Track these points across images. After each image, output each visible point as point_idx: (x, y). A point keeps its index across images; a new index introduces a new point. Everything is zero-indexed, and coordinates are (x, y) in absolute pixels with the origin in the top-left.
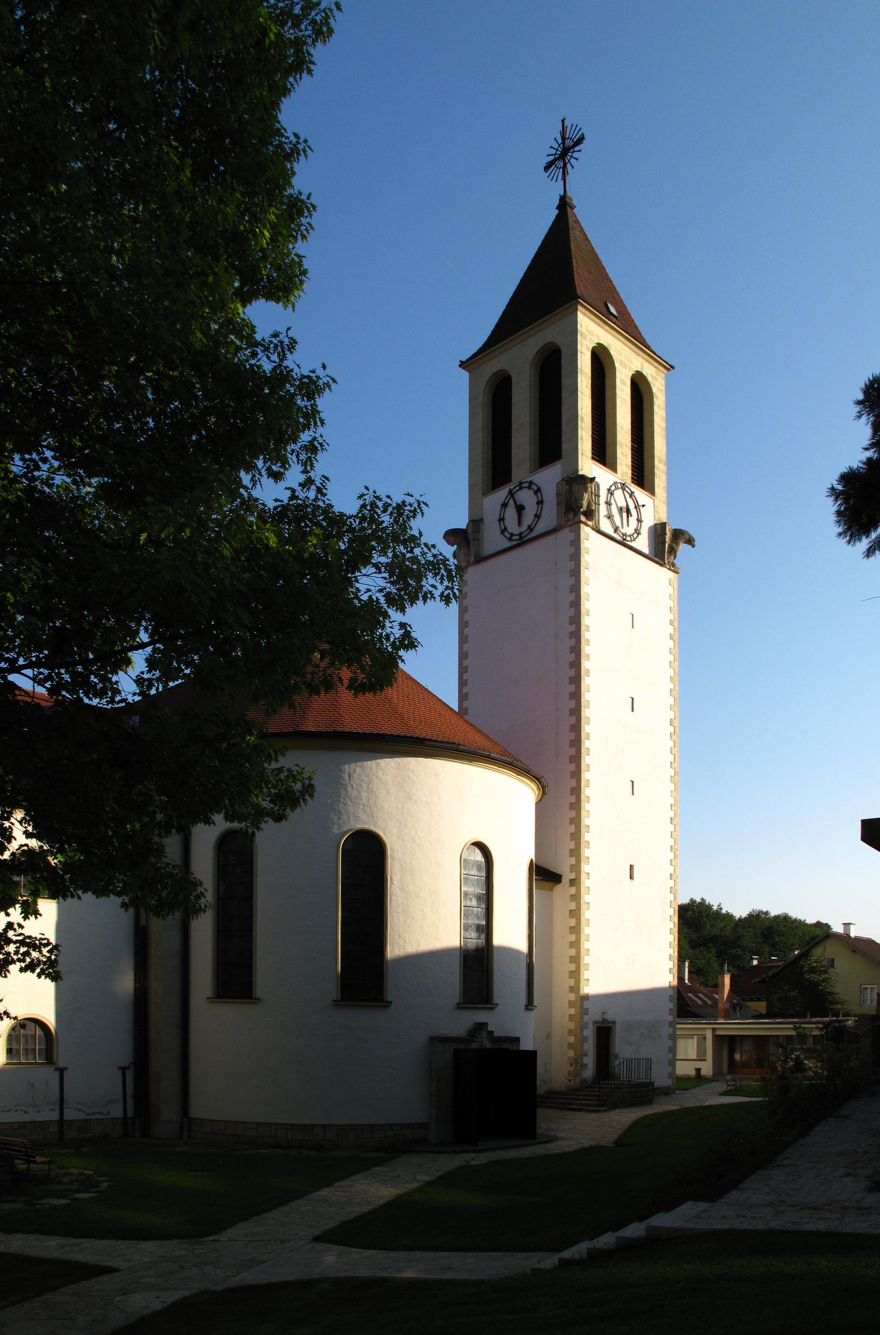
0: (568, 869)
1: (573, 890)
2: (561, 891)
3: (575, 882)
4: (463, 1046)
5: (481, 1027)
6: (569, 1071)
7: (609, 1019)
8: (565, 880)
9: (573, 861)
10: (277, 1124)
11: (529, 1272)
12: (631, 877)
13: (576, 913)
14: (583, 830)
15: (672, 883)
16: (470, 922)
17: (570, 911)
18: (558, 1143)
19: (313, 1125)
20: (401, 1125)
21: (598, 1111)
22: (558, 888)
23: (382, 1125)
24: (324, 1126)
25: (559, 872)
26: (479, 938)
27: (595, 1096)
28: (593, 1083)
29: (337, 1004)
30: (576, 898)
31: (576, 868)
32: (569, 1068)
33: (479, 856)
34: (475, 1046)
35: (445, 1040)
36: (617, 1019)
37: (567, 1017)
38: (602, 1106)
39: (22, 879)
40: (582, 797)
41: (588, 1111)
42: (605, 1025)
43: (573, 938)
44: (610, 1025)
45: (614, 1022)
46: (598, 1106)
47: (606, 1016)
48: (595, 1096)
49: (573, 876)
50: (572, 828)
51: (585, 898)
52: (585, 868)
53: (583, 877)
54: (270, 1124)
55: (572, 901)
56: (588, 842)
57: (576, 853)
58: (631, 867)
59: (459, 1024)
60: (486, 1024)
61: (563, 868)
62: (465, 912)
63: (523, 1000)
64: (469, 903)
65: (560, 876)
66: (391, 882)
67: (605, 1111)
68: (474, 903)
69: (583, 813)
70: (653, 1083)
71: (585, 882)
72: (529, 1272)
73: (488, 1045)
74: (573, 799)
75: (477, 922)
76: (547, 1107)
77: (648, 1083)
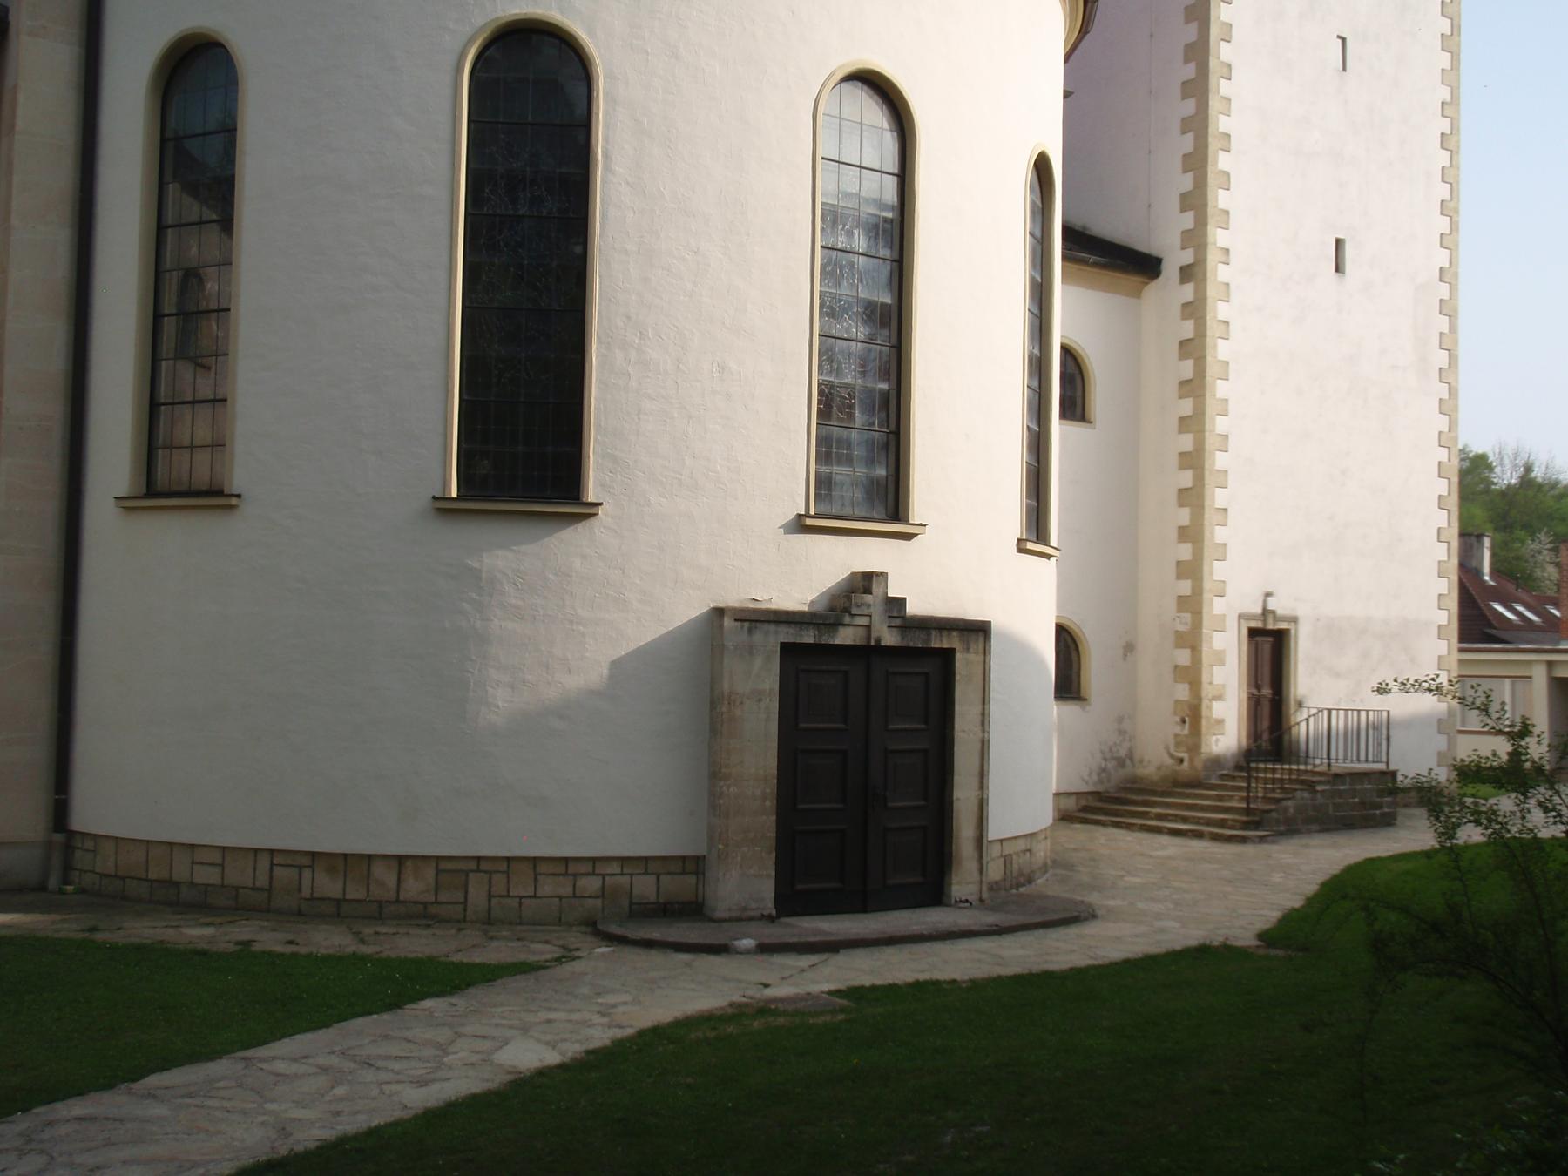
0: (1177, 241)
1: (1188, 292)
2: (1167, 292)
3: (1190, 273)
4: (809, 637)
5: (865, 582)
6: (1176, 736)
7: (1280, 612)
8: (1170, 270)
9: (1188, 220)
10: (272, 852)
11: (1443, 775)
12: (1339, 268)
13: (1193, 348)
14: (1213, 144)
15: (1444, 291)
16: (845, 290)
17: (1182, 343)
18: (1090, 929)
19: (370, 857)
20: (624, 861)
21: (1243, 840)
22: (1153, 290)
23: (566, 860)
24: (401, 860)
25: (1155, 252)
26: (870, 340)
27: (1239, 789)
28: (1238, 768)
29: (444, 509)
30: (1195, 310)
31: (1196, 238)
32: (1178, 729)
33: (874, 114)
34: (845, 636)
35: (756, 619)
36: (1301, 611)
37: (1171, 605)
38: (1256, 825)
39: (1186, 732)
40: (1213, 63)
41: (1216, 838)
42: (1270, 626)
43: (1186, 407)
45: (1294, 620)
46: (1246, 826)
47: (1272, 604)
48: (1239, 789)
49: (1187, 257)
50: (1187, 143)
51: (1219, 310)
52: (1218, 237)
53: (1213, 257)
54: (256, 851)
55: (1184, 317)
56: (1227, 174)
57: (1195, 201)
58: (1339, 243)
60: (884, 575)
61: (1163, 236)
62: (832, 264)
63: (1013, 522)
64: (842, 242)
65: (1158, 261)
66: (607, 168)
67: (1262, 839)
68: (860, 242)
69: (1214, 104)
70: (1393, 774)
71: (1219, 273)
72: (1443, 775)
73: (890, 639)
74: (1190, 71)
75: (864, 295)
76: (1117, 825)
77: (1383, 773)
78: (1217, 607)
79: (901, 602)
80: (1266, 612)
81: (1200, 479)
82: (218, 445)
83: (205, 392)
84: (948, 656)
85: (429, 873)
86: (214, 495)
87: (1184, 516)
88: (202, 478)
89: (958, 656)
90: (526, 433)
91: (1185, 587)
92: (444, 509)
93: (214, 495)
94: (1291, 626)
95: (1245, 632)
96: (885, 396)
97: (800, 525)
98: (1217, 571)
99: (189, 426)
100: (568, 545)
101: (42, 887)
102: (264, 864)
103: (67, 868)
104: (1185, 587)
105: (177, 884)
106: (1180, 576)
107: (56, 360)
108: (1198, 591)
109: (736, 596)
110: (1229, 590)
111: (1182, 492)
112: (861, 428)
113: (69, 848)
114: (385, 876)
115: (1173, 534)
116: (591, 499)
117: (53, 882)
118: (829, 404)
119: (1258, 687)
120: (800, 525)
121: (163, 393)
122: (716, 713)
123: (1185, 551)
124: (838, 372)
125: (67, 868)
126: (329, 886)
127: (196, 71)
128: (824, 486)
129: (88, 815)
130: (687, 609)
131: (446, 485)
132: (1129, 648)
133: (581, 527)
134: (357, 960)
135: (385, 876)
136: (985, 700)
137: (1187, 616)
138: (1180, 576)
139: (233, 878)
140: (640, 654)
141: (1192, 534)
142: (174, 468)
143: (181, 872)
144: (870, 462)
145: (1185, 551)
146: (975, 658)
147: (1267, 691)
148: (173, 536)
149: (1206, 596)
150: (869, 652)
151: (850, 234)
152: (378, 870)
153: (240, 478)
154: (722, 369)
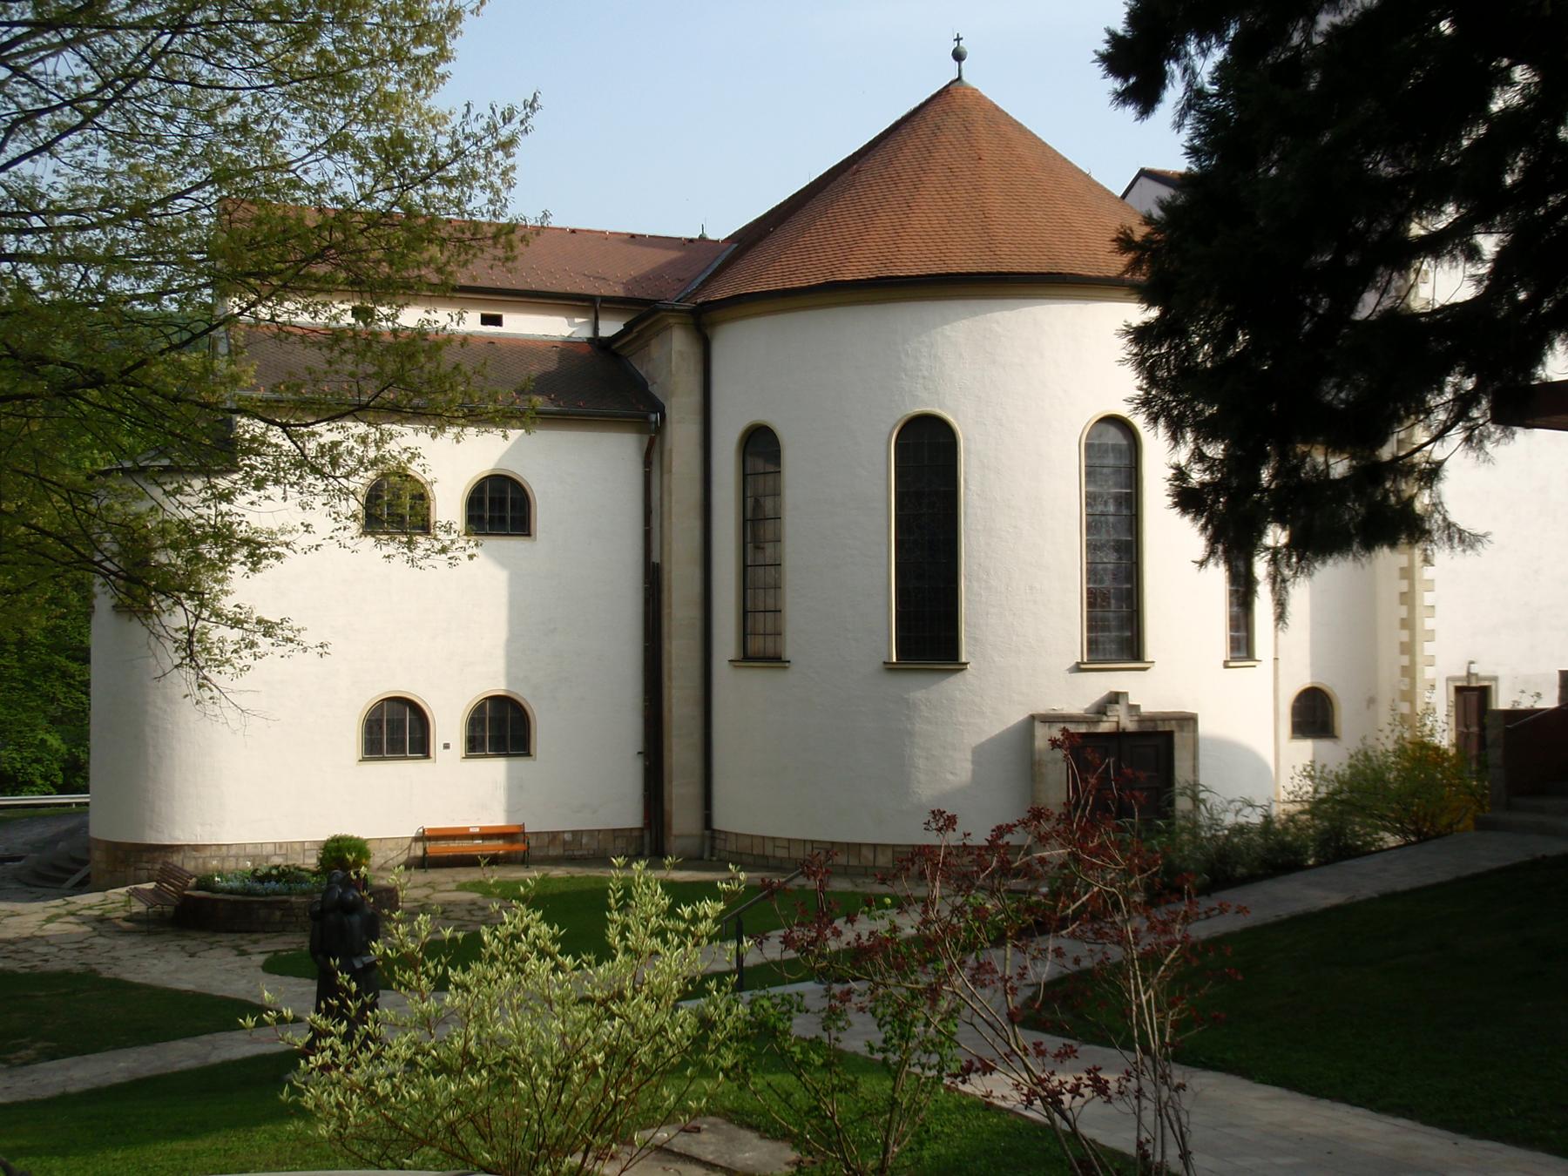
5: (1115, 698)
7: (1482, 674)
29: (889, 667)
33: (1114, 436)
34: (1105, 727)
37: (1398, 672)
42: (1474, 684)
44: (1486, 683)
45: (1495, 679)
47: (1474, 669)
59: (1079, 695)
60: (1126, 694)
78: (1427, 673)
79: (1137, 707)
80: (1469, 675)
81: (1412, 586)
82: (778, 634)
83: (770, 628)
84: (1169, 736)
85: (889, 853)
86: (775, 660)
87: (1403, 612)
88: (770, 652)
89: (1177, 735)
90: (929, 625)
91: (1405, 660)
92: (889, 667)
93: (775, 660)
94: (1492, 684)
95: (1452, 690)
96: (1130, 591)
97: (1078, 668)
98: (1426, 649)
99: (760, 622)
100: (951, 686)
101: (701, 858)
102: (809, 847)
103: (712, 848)
104: (1405, 660)
105: (767, 857)
106: (1403, 652)
107: (696, 587)
108: (1413, 663)
109: (1042, 708)
110: (1438, 661)
111: (1402, 594)
112: (1113, 610)
113: (713, 838)
114: (868, 854)
115: (1397, 624)
116: (964, 660)
117: (706, 856)
118: (1095, 599)
119: (1467, 726)
120: (1078, 668)
121: (749, 606)
122: (1031, 767)
123: (1404, 636)
124: (1102, 581)
125: (712, 848)
126: (841, 859)
127: (761, 445)
128: (1093, 646)
129: (721, 822)
130: (1016, 716)
131: (890, 656)
132: (1372, 701)
133: (959, 675)
134: (853, 894)
135: (868, 854)
136: (1195, 757)
137: (1407, 680)
138: (1403, 652)
139: (794, 854)
140: (992, 741)
141: (1408, 624)
142: (756, 645)
143: (769, 851)
144: (1121, 628)
145: (1404, 636)
146: (1187, 735)
147: (1474, 729)
148: (758, 680)
149: (1419, 667)
150: (1119, 736)
151: (1106, 503)
152: (865, 851)
153: (788, 653)
154: (1031, 588)
